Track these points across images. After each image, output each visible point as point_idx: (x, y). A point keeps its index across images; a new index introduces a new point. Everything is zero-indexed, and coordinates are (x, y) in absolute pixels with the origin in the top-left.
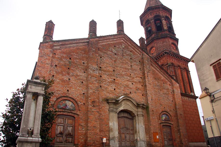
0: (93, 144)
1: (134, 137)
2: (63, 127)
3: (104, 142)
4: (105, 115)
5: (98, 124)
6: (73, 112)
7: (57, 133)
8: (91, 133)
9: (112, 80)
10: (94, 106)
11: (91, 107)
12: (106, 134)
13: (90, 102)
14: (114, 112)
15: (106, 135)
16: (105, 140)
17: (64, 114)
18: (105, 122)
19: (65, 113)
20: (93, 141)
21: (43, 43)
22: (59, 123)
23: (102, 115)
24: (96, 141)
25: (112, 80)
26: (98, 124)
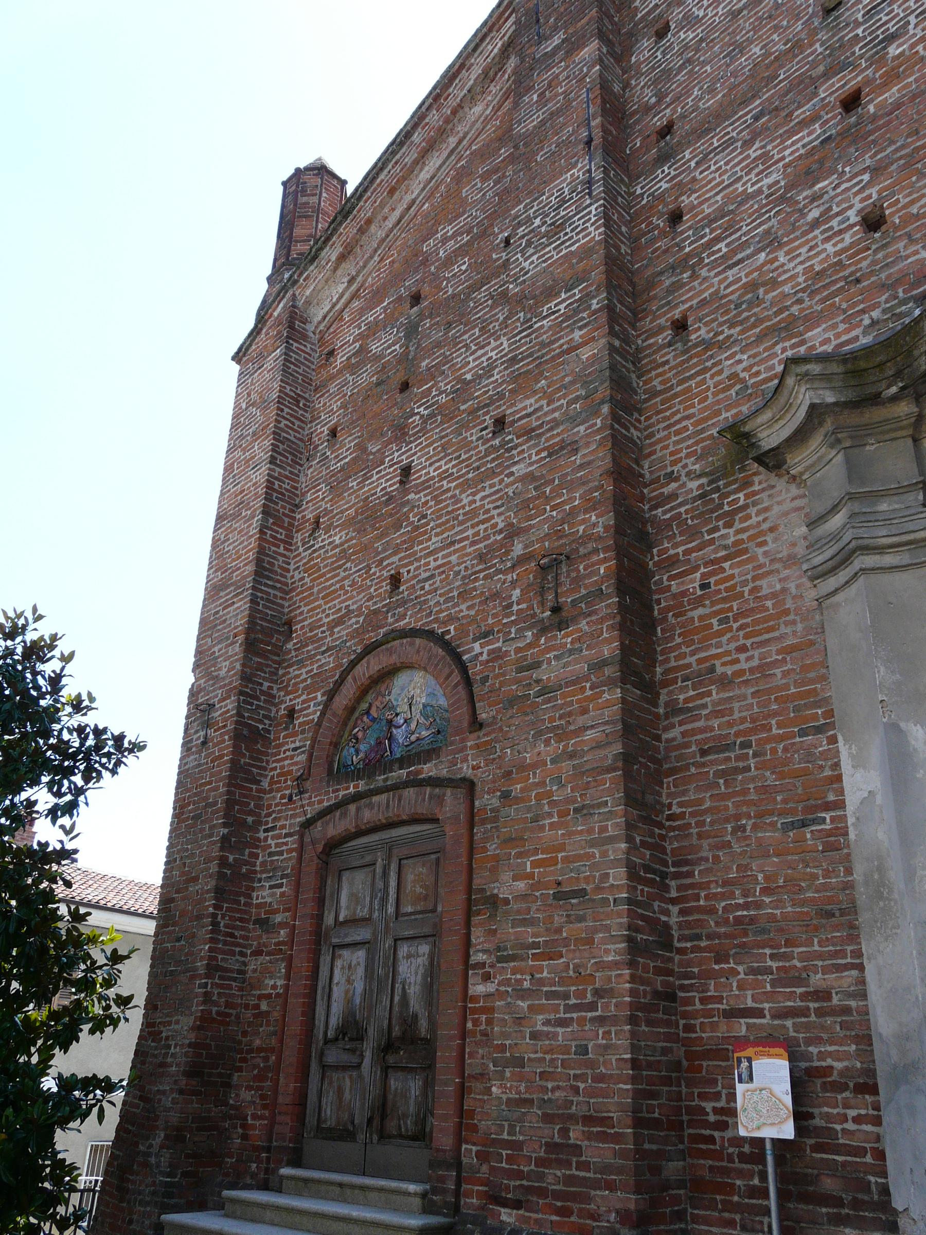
0: (553, 1177)
1: (367, 958)
2: (368, 951)
3: (759, 1142)
4: (763, 669)
5: (612, 840)
6: (429, 770)
7: (326, 1033)
8: (522, 994)
9: (834, 121)
10: (556, 610)
11: (530, 646)
12: (817, 980)
13: (517, 593)
14: (870, 561)
15: (823, 995)
16: (783, 1089)
17: (367, 815)
18: (770, 778)
19: (371, 806)
20: (548, 1118)
21: (244, 355)
22: (346, 922)
23: (725, 682)
24: (588, 1120)
25: (834, 121)
26: (612, 840)
